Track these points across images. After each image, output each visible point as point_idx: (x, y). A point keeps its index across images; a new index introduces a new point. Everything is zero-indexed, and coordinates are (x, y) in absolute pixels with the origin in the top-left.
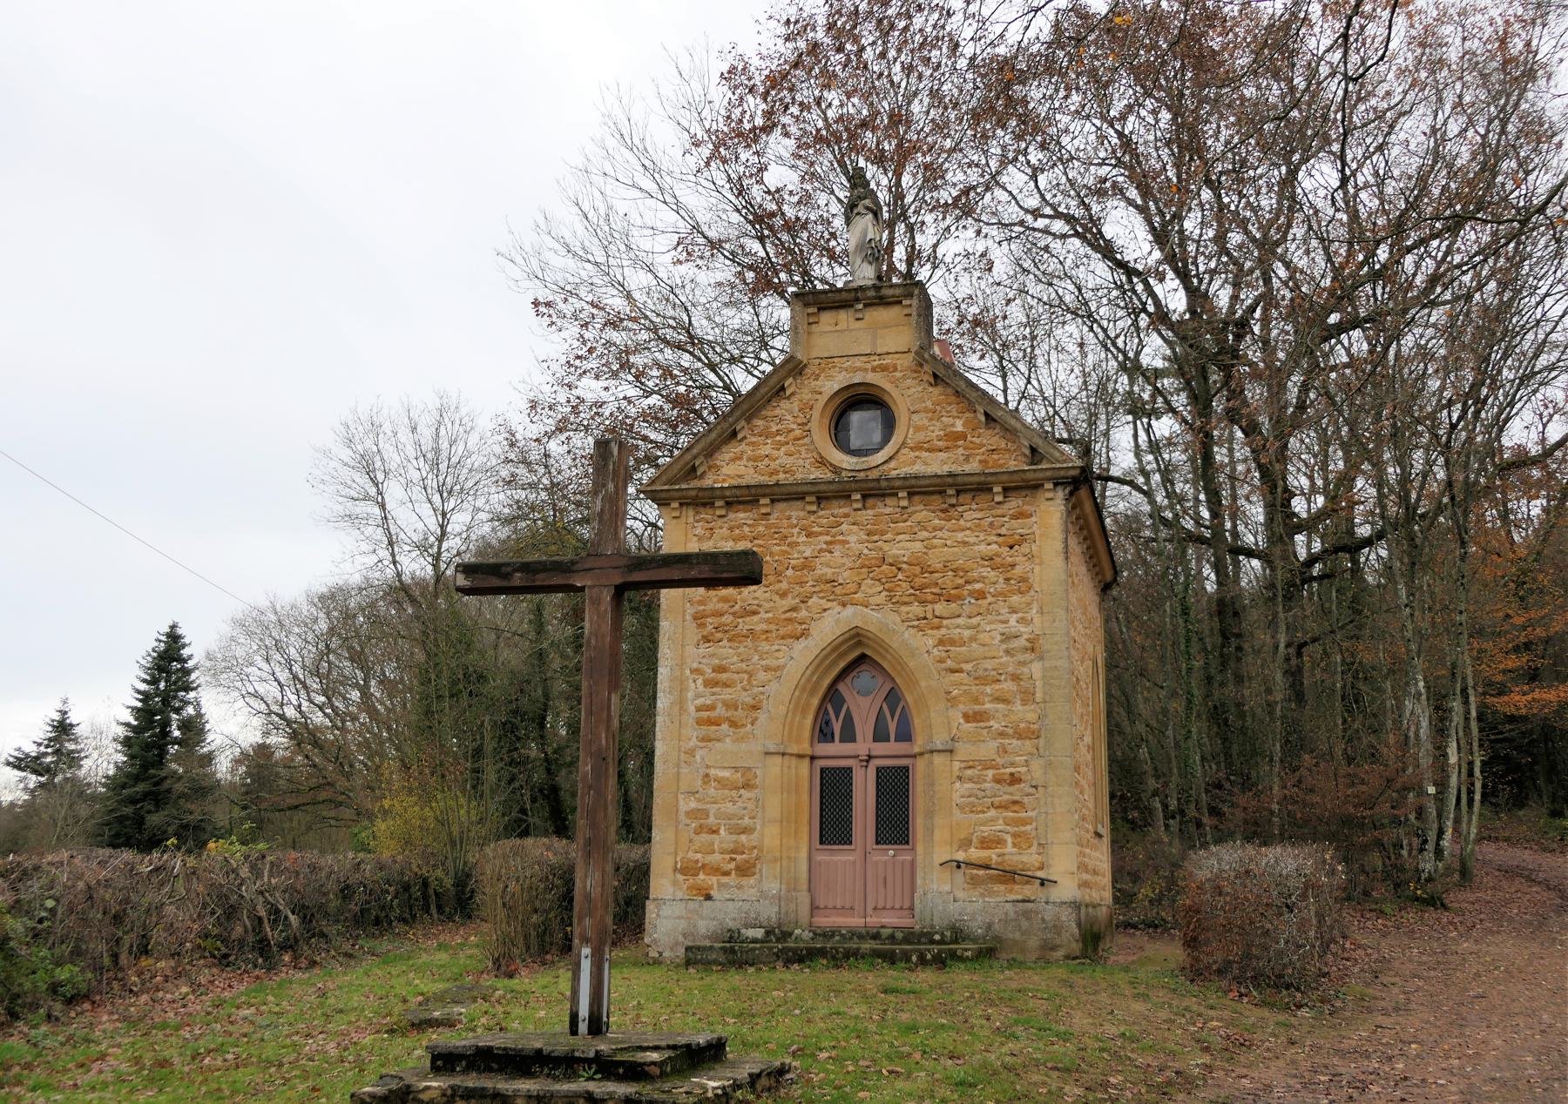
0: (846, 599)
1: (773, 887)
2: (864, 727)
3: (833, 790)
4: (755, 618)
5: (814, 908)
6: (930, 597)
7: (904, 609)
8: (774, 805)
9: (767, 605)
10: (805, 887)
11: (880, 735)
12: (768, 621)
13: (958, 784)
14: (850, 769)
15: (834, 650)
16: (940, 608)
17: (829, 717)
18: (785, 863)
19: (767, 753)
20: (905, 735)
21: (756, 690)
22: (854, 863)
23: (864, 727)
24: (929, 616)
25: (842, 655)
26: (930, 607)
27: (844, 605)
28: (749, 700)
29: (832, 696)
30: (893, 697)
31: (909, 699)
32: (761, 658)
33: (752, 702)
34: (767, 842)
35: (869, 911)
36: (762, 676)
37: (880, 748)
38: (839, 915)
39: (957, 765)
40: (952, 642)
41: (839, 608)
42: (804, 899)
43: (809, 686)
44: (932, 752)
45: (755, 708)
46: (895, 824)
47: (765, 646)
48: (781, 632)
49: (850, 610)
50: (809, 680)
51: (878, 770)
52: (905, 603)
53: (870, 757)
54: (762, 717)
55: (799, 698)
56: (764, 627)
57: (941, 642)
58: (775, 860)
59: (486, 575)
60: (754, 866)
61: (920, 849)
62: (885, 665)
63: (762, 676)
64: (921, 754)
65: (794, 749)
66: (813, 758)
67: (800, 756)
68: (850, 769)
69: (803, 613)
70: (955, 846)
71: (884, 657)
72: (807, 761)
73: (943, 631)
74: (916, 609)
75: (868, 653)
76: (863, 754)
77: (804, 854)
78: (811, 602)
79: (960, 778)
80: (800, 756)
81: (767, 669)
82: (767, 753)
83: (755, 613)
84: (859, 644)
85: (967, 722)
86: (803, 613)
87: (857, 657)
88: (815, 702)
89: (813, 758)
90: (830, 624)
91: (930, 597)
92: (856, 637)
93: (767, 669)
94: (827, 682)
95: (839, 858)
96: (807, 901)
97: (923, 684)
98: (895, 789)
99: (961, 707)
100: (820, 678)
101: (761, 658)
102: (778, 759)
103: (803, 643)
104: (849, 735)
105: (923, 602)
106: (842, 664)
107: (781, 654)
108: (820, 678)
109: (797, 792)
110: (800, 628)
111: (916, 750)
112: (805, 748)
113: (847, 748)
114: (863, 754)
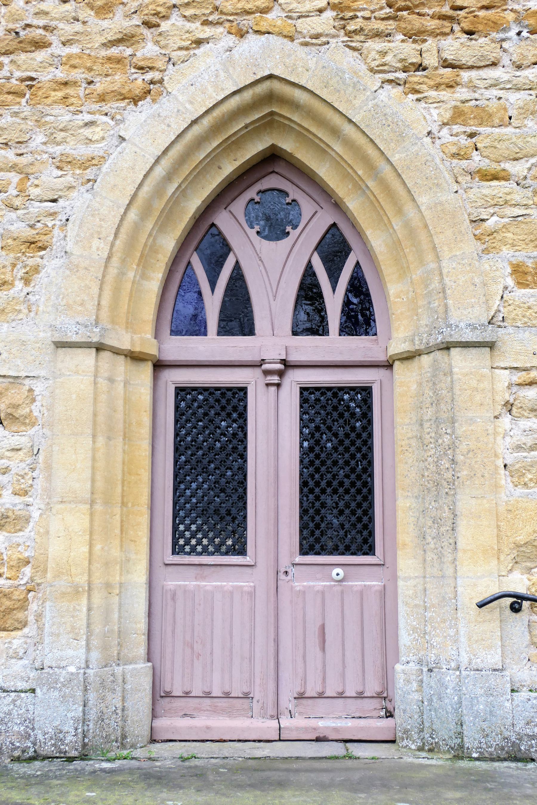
0: (248, 21)
1: (70, 655)
2: (273, 302)
3: (207, 433)
4: (41, 55)
5: (159, 695)
6: (432, 24)
7: (375, 46)
8: (73, 463)
9: (68, 29)
10: (142, 651)
11: (310, 317)
12: (69, 63)
13: (506, 420)
14: (241, 392)
15: (217, 128)
16: (454, 46)
17: (203, 285)
18: (97, 599)
19: (60, 345)
20: (359, 318)
21: (36, 208)
22: (252, 594)
23: (273, 302)
24: (431, 60)
25: (232, 144)
26: (431, 43)
27: (241, 34)
28: (19, 228)
29: (206, 242)
30: (334, 249)
31: (377, 241)
32: (51, 140)
33: (29, 233)
34: (55, 549)
35: (287, 701)
36: (50, 178)
37: (309, 348)
38: (215, 711)
39: (504, 377)
40: (484, 116)
41: (231, 40)
42: (139, 675)
43: (159, 205)
44: (447, 347)
45: (35, 245)
46: (341, 509)
47: (62, 115)
48: (99, 87)
49: (253, 42)
50: (159, 191)
51: (306, 392)
52: (378, 35)
53: (288, 365)
54: (51, 265)
55: (137, 228)
56: (60, 74)
57: (458, 115)
58: (76, 592)
59: (181, 788)
60: (24, 604)
61: (407, 565)
62: (324, 171)
63: (50, 178)
64: (408, 357)
65: (124, 341)
66: (159, 366)
67: (135, 357)
68: (241, 392)
69: (148, 50)
70: (507, 561)
71: (322, 151)
72: (148, 368)
73: (462, 93)
74: (402, 49)
75: (287, 145)
76: (272, 368)
77: (139, 576)
78: (165, 26)
79: (509, 406)
80: (135, 357)
81: (63, 163)
82: (60, 345)
83: (39, 45)
84: (270, 122)
85: (521, 284)
86: (148, 50)
87: (262, 160)
88: (169, 243)
89: (159, 366)
90: (209, 75)
91: (432, 24)
92: (268, 103)
93: (63, 163)
94: (194, 204)
95: (214, 584)
96: (146, 684)
97: (423, 200)
98: (340, 438)
99: (506, 252)
100: (182, 193)
101: (51, 140)
102: (88, 358)
103: (137, 118)
104: (238, 318)
105: (415, 36)
106: (229, 168)
107: (96, 133)
108: (182, 193)
109: (127, 437)
110: (140, 80)
111: (397, 347)
112: (144, 340)
113: (236, 347)
114: (272, 368)
